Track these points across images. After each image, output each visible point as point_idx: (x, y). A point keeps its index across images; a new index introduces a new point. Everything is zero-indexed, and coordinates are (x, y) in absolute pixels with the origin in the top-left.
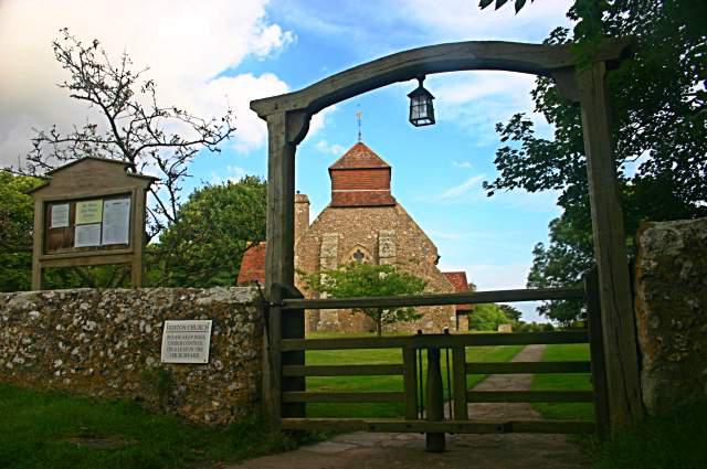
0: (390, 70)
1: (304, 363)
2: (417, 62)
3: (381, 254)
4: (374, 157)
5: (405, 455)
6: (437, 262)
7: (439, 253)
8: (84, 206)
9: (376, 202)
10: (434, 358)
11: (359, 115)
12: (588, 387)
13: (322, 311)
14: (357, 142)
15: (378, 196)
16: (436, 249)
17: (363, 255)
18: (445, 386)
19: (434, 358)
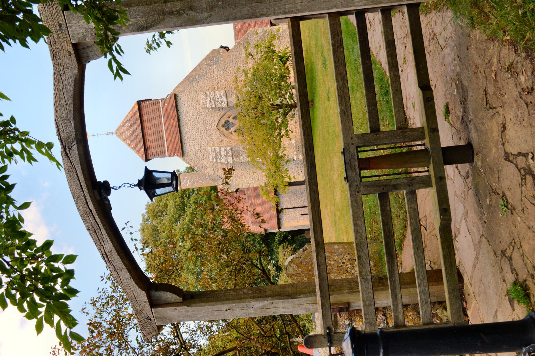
0: (98, 220)
1: (379, 194)
2: (94, 211)
3: (224, 105)
4: (128, 119)
5: (489, 199)
6: (227, 49)
7: (218, 47)
8: (145, 302)
9: (173, 113)
10: (366, 164)
11: (135, 245)
12: (403, 193)
13: (326, 240)
14: (115, 135)
15: (167, 112)
16: (214, 51)
17: (227, 122)
18: (393, 151)
19: (366, 164)
